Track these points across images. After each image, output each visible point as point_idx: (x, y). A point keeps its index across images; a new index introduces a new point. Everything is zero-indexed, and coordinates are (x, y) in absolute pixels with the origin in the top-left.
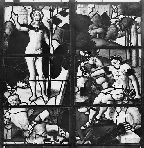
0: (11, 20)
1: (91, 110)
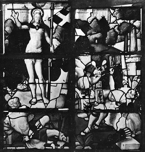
0: (12, 18)
1: (91, 116)
